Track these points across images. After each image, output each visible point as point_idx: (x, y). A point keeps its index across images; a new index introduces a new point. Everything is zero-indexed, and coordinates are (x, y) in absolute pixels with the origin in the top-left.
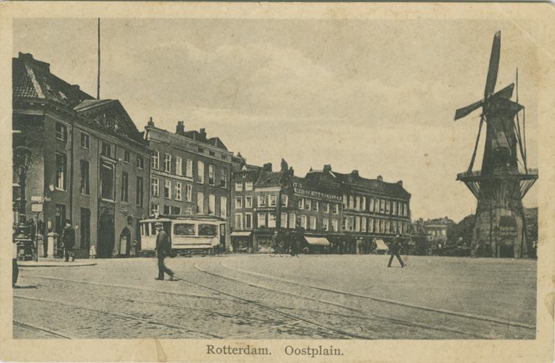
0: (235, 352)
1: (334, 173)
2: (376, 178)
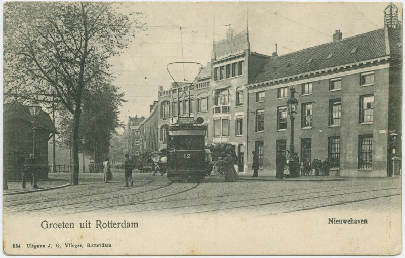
2: (330, 40)
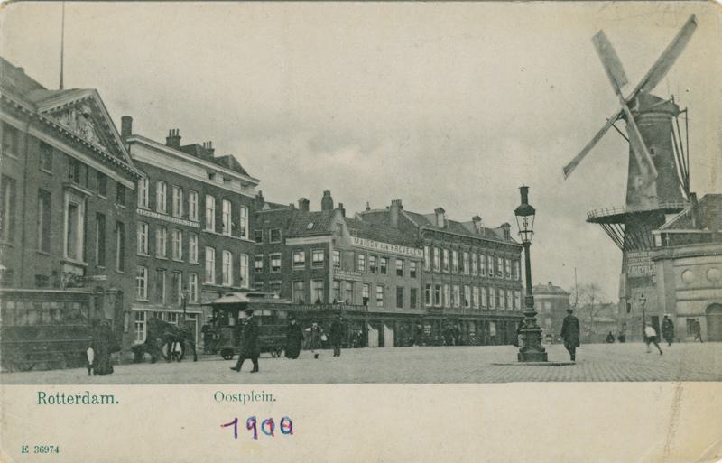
1: (409, 213)
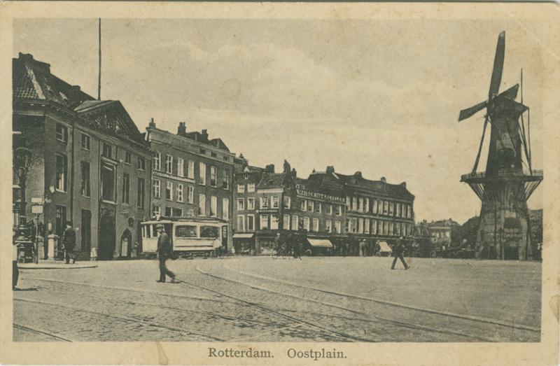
0: (237, 355)
1: (337, 175)
2: (379, 179)
